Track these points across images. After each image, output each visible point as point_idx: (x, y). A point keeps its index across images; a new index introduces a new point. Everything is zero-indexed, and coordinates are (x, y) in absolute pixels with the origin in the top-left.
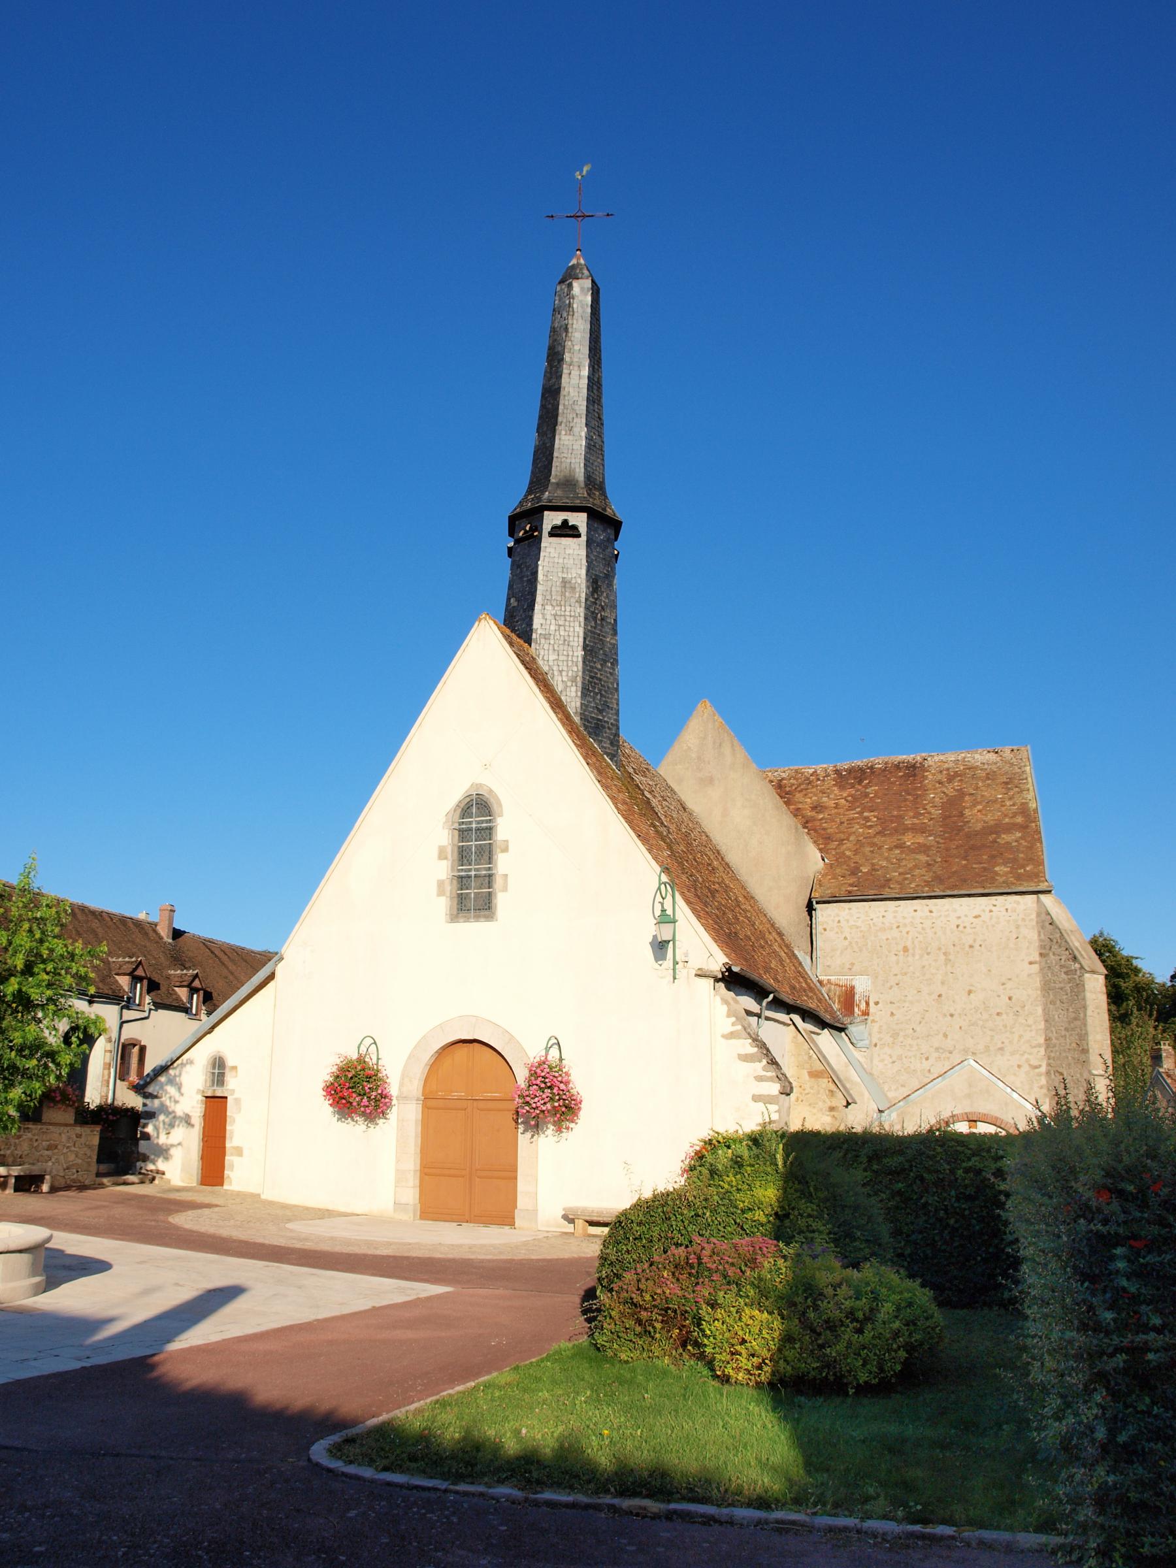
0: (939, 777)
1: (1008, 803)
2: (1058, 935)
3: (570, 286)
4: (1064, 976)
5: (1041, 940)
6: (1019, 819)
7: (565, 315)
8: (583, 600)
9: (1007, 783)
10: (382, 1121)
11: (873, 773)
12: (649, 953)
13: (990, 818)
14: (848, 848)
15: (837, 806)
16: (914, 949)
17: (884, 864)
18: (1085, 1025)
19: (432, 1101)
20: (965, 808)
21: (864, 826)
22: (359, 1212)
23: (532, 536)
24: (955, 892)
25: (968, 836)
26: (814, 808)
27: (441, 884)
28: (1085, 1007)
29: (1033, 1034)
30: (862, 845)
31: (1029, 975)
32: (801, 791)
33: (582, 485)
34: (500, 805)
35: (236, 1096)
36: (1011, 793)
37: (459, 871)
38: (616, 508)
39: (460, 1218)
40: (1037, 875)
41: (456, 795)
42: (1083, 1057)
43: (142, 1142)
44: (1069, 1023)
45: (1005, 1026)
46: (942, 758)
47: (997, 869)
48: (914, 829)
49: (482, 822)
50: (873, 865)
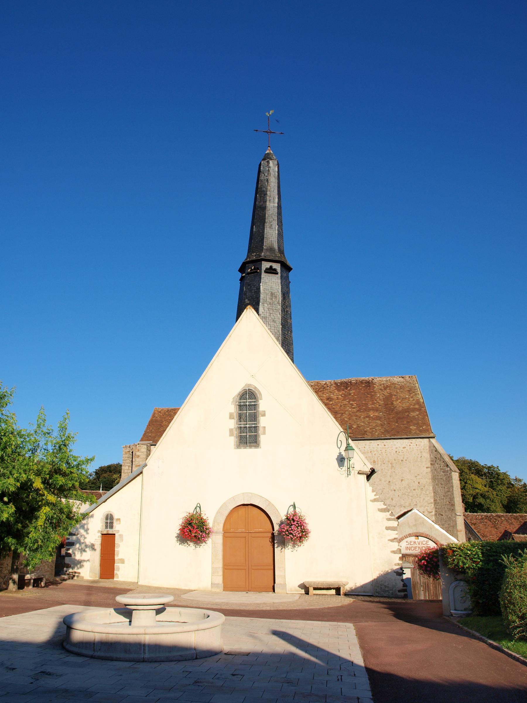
0: (380, 387)
1: (411, 399)
3: (268, 162)
4: (442, 473)
5: (431, 458)
6: (417, 406)
7: (266, 174)
8: (280, 302)
9: (409, 391)
10: (204, 544)
11: (351, 384)
12: (336, 463)
13: (405, 405)
14: (345, 417)
15: (338, 398)
16: (378, 461)
17: (363, 424)
18: (453, 494)
19: (227, 534)
20: (393, 401)
21: (351, 408)
22: (193, 589)
23: (257, 272)
24: (396, 437)
25: (397, 413)
26: (328, 399)
27: (231, 430)
28: (452, 487)
29: (429, 498)
30: (352, 416)
31: (426, 473)
32: (321, 391)
33: (277, 251)
34: (261, 394)
35: (119, 534)
36: (412, 395)
37: (239, 424)
38: (289, 263)
39: (248, 589)
40: (428, 430)
41: (238, 389)
42: (452, 508)
43: (66, 558)
44: (445, 493)
45: (417, 495)
46: (380, 379)
47: (411, 427)
48: (373, 409)
49: (253, 402)
50: (358, 424)
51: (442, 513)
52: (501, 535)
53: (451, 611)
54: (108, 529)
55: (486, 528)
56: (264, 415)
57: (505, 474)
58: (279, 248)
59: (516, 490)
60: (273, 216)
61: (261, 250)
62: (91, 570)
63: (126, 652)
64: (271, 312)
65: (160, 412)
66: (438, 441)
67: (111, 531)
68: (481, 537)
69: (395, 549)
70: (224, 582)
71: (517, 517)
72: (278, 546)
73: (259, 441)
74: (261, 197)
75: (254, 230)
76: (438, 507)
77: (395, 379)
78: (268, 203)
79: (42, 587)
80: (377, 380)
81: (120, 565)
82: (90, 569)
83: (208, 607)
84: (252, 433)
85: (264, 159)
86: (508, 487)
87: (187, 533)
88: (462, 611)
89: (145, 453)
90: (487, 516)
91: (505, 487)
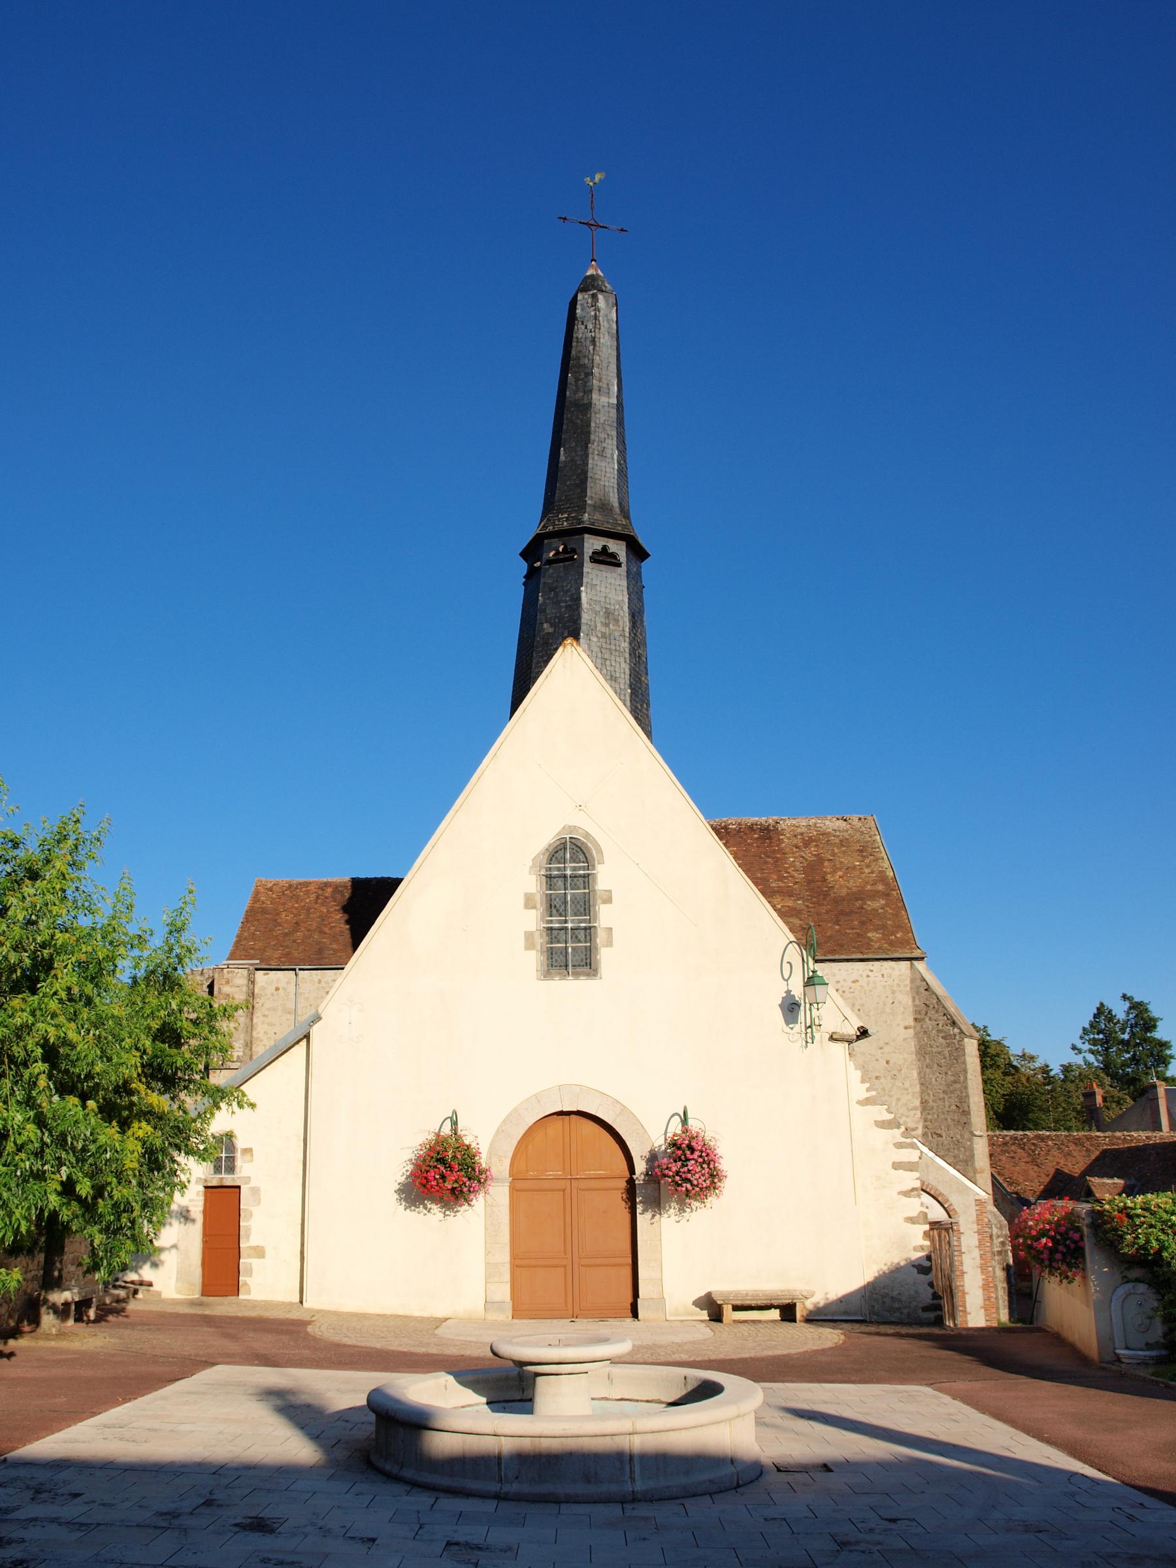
0: (795, 841)
1: (867, 871)
2: (935, 1001)
3: (594, 297)
4: (941, 1040)
5: (915, 1006)
6: (880, 887)
7: (590, 326)
9: (861, 851)
10: (466, 1207)
12: (778, 1015)
13: (854, 884)
18: (966, 1088)
19: (519, 1183)
23: (572, 559)
24: (837, 957)
25: (837, 901)
27: (529, 936)
28: (965, 1071)
29: (910, 1097)
31: (905, 1040)
33: (618, 510)
34: (600, 851)
35: (252, 1184)
40: (908, 942)
41: (546, 837)
42: (964, 1119)
44: (948, 1086)
47: (870, 935)
49: (580, 868)
51: (939, 1132)
52: (1047, 1180)
53: (1118, 1351)
54: (223, 1176)
55: (1016, 1165)
56: (609, 900)
57: (999, 1043)
58: (620, 504)
59: (1024, 1080)
60: (608, 428)
61: (582, 508)
62: (181, 1275)
63: (587, 1479)
64: (607, 656)
65: (270, 889)
66: (930, 967)
67: (228, 1180)
68: (1005, 1185)
69: (914, 1214)
70: (513, 1298)
71: (1079, 1139)
72: (644, 1211)
73: (598, 962)
74: (577, 380)
75: (562, 458)
76: (930, 1117)
77: (827, 823)
78: (595, 396)
79: (89, 1321)
80: (786, 824)
81: (255, 1263)
82: (178, 1272)
83: (671, 1359)
84: (579, 941)
85: (584, 289)
86: (1005, 1074)
87: (434, 1183)
88: (1141, 1350)
89: (245, 989)
90: (1016, 1138)
91: (999, 1072)
